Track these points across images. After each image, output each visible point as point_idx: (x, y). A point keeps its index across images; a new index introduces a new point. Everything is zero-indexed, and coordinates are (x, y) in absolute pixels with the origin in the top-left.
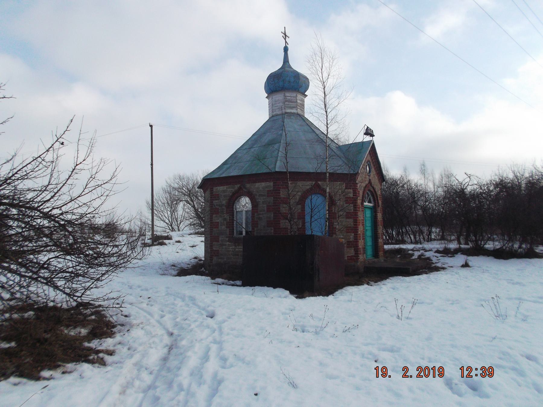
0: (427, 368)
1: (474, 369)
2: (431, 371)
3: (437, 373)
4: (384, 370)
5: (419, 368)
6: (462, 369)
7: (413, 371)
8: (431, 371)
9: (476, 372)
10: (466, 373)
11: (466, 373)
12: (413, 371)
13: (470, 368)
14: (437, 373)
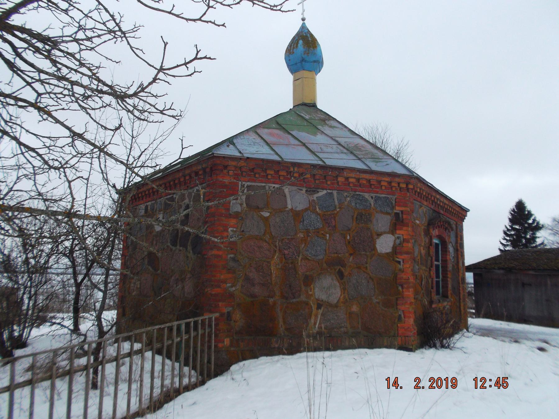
0: (439, 378)
1: (488, 380)
2: (444, 382)
3: (450, 384)
4: (454, 381)
5: (431, 379)
6: (475, 379)
7: (425, 383)
8: (444, 382)
9: (490, 383)
10: (479, 384)
11: (479, 384)
12: (425, 383)
13: (483, 379)
14: (450, 384)
